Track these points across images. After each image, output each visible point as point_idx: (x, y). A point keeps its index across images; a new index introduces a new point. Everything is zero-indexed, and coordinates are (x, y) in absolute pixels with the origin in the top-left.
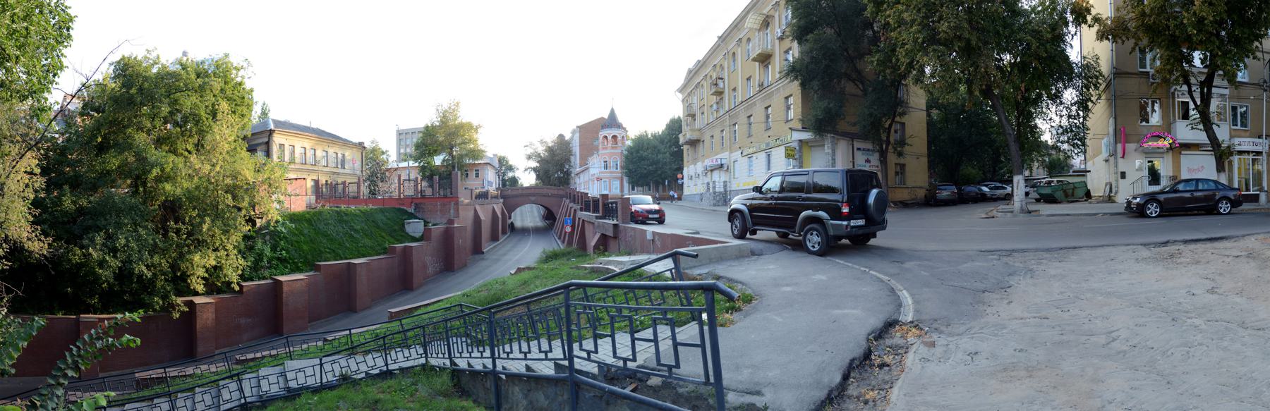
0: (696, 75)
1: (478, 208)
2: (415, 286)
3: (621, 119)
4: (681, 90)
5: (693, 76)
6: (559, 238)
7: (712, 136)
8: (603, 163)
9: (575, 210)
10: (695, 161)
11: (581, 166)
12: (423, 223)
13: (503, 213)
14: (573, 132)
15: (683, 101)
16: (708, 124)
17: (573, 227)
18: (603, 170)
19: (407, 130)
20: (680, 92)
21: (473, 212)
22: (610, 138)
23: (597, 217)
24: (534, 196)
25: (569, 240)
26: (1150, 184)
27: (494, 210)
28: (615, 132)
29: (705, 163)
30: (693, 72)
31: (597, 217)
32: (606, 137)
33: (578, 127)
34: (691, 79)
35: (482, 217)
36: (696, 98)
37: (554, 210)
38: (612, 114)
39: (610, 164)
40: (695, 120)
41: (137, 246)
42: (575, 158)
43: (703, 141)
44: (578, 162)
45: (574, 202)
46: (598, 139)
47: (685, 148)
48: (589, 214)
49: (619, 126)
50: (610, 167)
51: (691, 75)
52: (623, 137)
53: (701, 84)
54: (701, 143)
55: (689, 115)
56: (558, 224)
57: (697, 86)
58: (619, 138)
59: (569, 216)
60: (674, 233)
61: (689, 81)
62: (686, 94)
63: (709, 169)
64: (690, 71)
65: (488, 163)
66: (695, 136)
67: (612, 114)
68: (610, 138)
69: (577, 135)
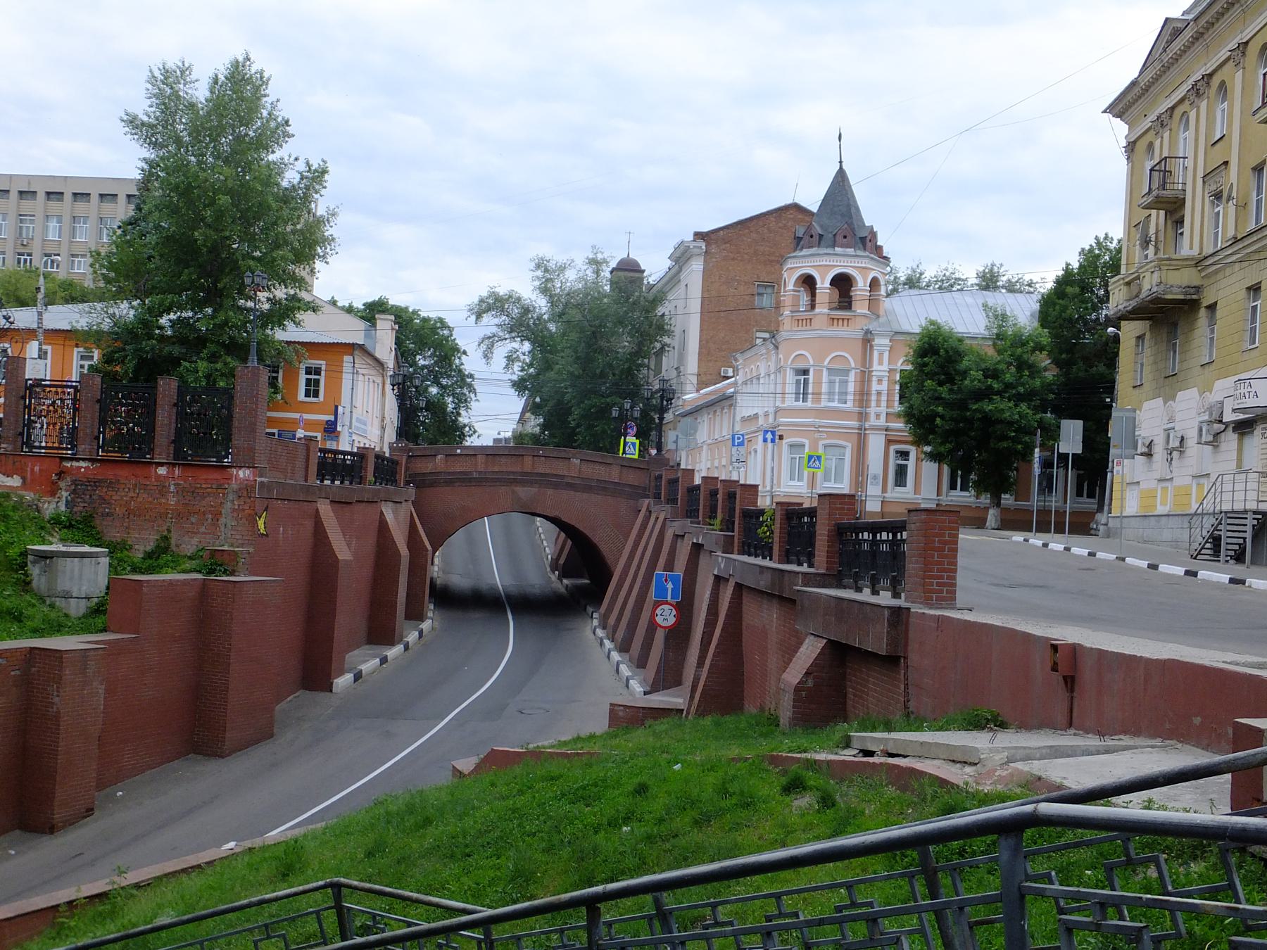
0: (1198, 47)
1: (325, 508)
2: (58, 815)
3: (871, 212)
4: (1121, 107)
5: (1184, 51)
6: (624, 648)
7: (1255, 289)
8: (790, 377)
9: (697, 548)
10: (1170, 382)
11: (702, 384)
12: (105, 561)
13: (413, 540)
14: (681, 257)
15: (1131, 147)
16: (1236, 241)
17: (685, 608)
18: (790, 402)
19: (30, 178)
20: (1119, 115)
21: (309, 525)
22: (823, 284)
23: (808, 579)
24: (531, 483)
25: (664, 660)
26: (905, 486)
27: (383, 526)
28: (845, 262)
29: (1215, 397)
30: (1188, 34)
31: (808, 579)
32: (808, 282)
33: (699, 235)
34: (1166, 68)
35: (342, 549)
36: (1190, 134)
37: (602, 538)
38: (840, 186)
39: (818, 383)
40: (1180, 222)
41: (8, 506)
42: (682, 357)
43: (1212, 307)
44: (692, 365)
45: (691, 513)
46: (774, 285)
47: (1129, 332)
48: (767, 563)
49: (866, 242)
50: (818, 394)
51: (1177, 45)
52: (874, 283)
53: (1216, 81)
54: (1203, 312)
55: (1158, 203)
56: (621, 591)
57: (1196, 91)
58: (861, 286)
59: (669, 566)
60: (989, 622)
61: (1166, 68)
62: (1147, 124)
63: (1229, 417)
64: (1171, 30)
65: (362, 348)
66: (1177, 282)
67: (840, 186)
68: (823, 284)
69: (696, 268)
